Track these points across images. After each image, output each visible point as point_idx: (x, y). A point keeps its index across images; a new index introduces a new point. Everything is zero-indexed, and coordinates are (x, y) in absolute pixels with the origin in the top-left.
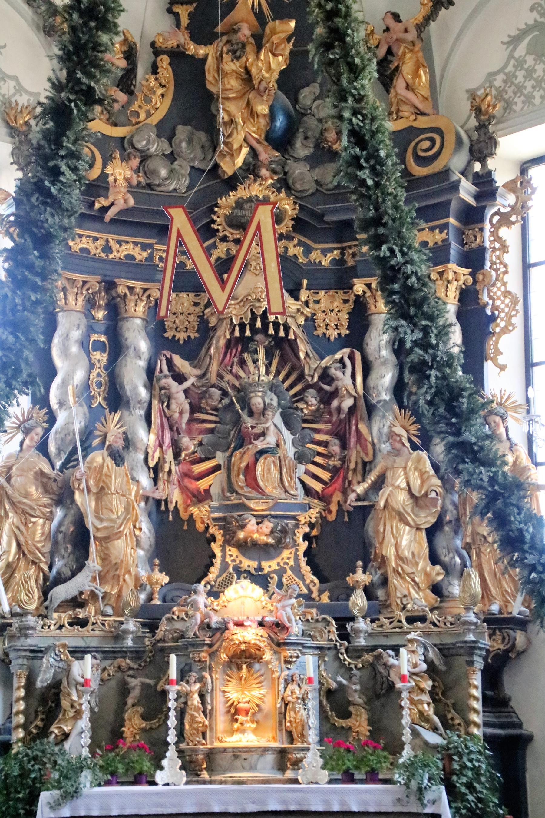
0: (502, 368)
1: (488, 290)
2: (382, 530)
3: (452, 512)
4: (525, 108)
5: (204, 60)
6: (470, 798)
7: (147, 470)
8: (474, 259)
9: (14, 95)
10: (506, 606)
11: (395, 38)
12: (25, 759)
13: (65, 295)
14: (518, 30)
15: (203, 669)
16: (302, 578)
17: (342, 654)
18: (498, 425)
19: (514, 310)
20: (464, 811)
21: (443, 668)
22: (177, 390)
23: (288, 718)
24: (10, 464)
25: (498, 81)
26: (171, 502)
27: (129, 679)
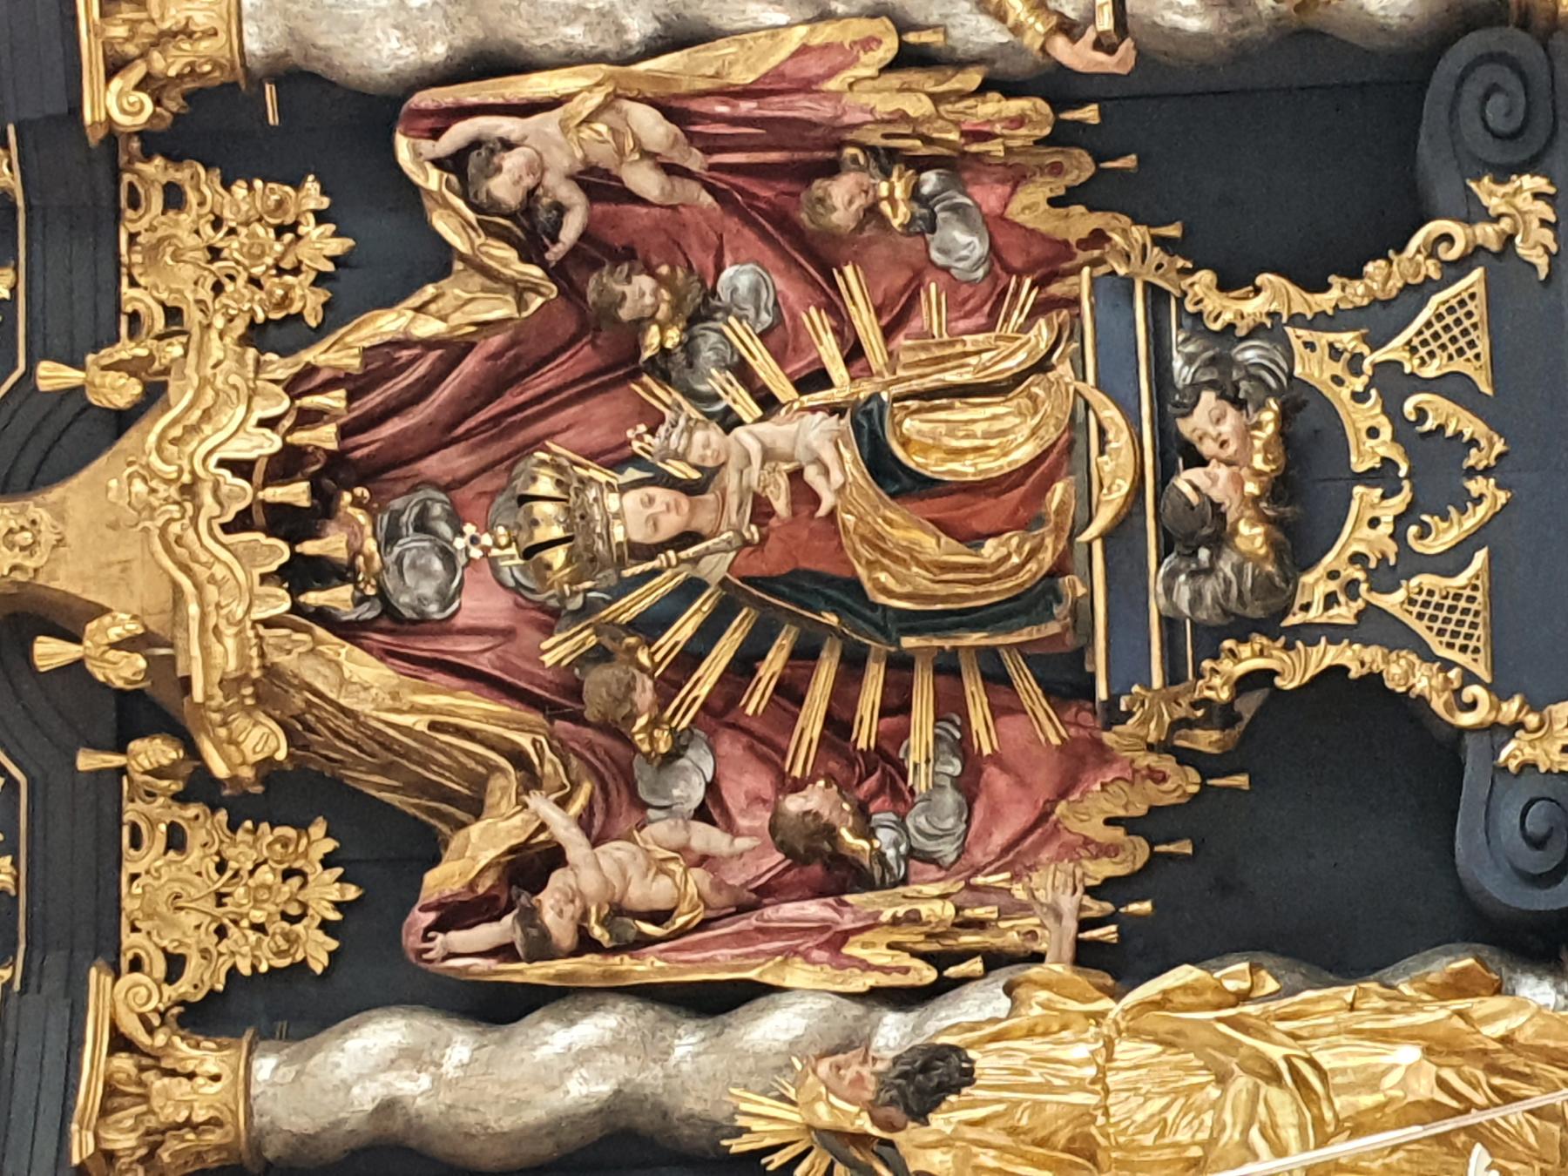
16: (1417, 292)
22: (591, 872)
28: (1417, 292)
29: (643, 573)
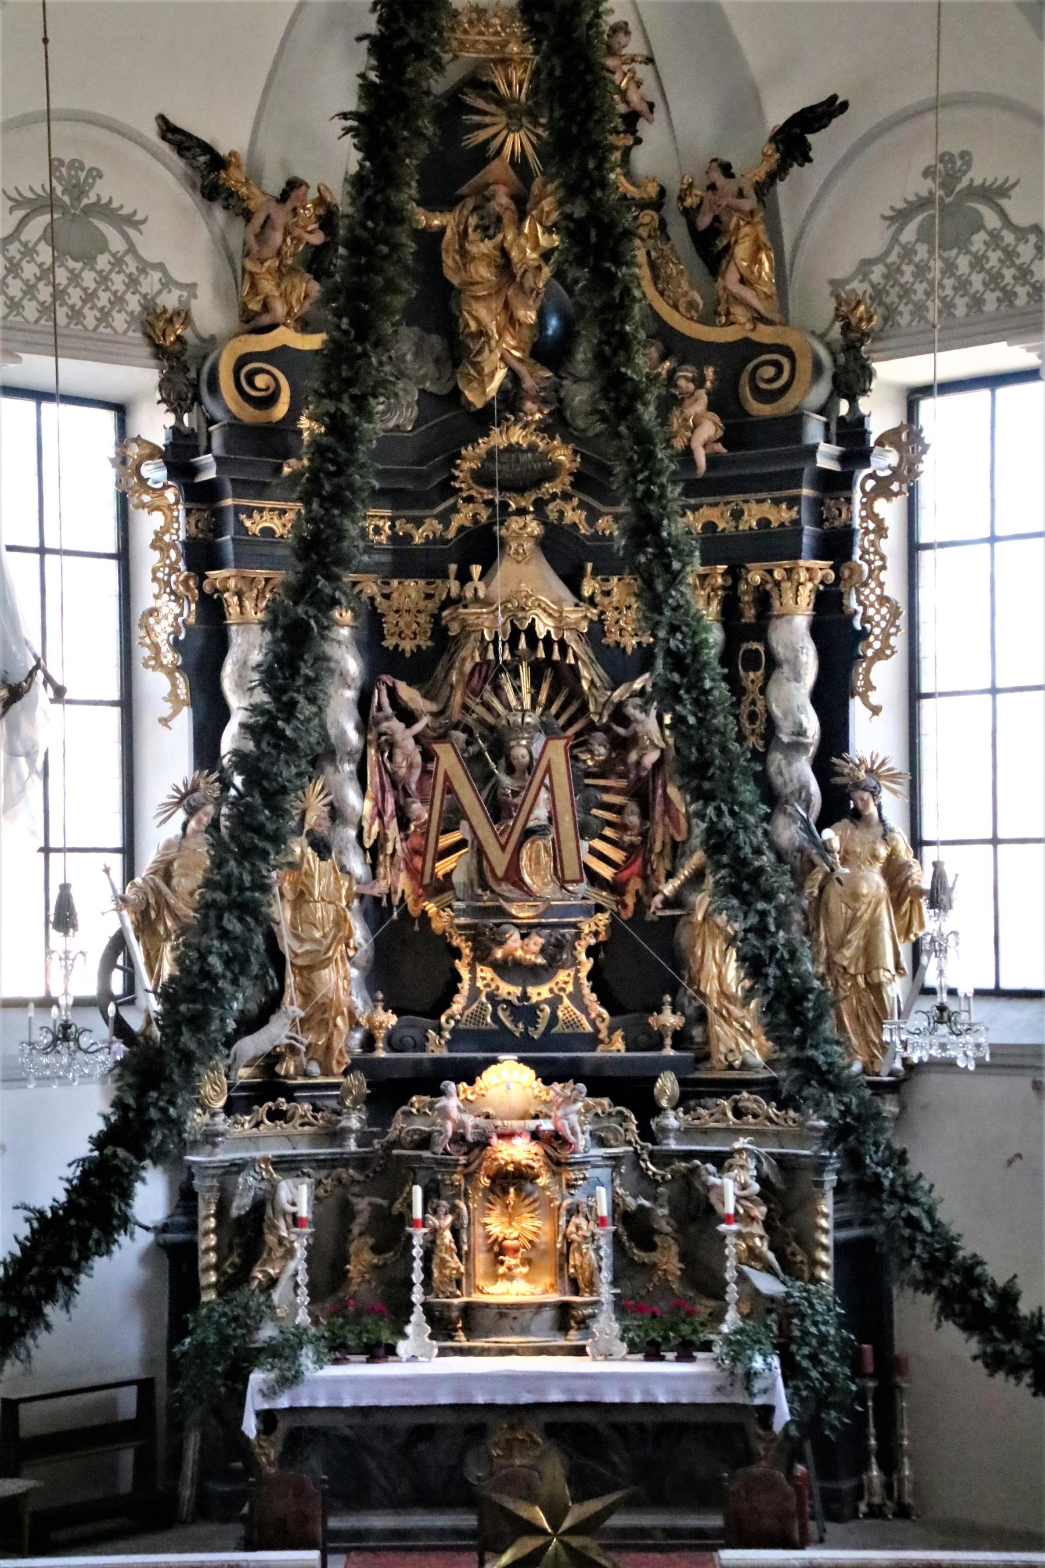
0: (876, 710)
1: (858, 593)
2: (699, 953)
3: (799, 924)
4: (915, 323)
6: (814, 1374)
7: (361, 851)
8: (836, 545)
9: (160, 292)
10: (872, 1063)
11: (724, 203)
12: (223, 1320)
13: (240, 600)
14: (906, 201)
15: (457, 1196)
16: (585, 1010)
17: (644, 1160)
18: (866, 804)
19: (893, 625)
20: (804, 1393)
21: (780, 1186)
22: (404, 736)
23: (572, 1262)
24: (169, 857)
25: (877, 273)
26: (396, 892)
27: (354, 1200)
28: (585, 1010)
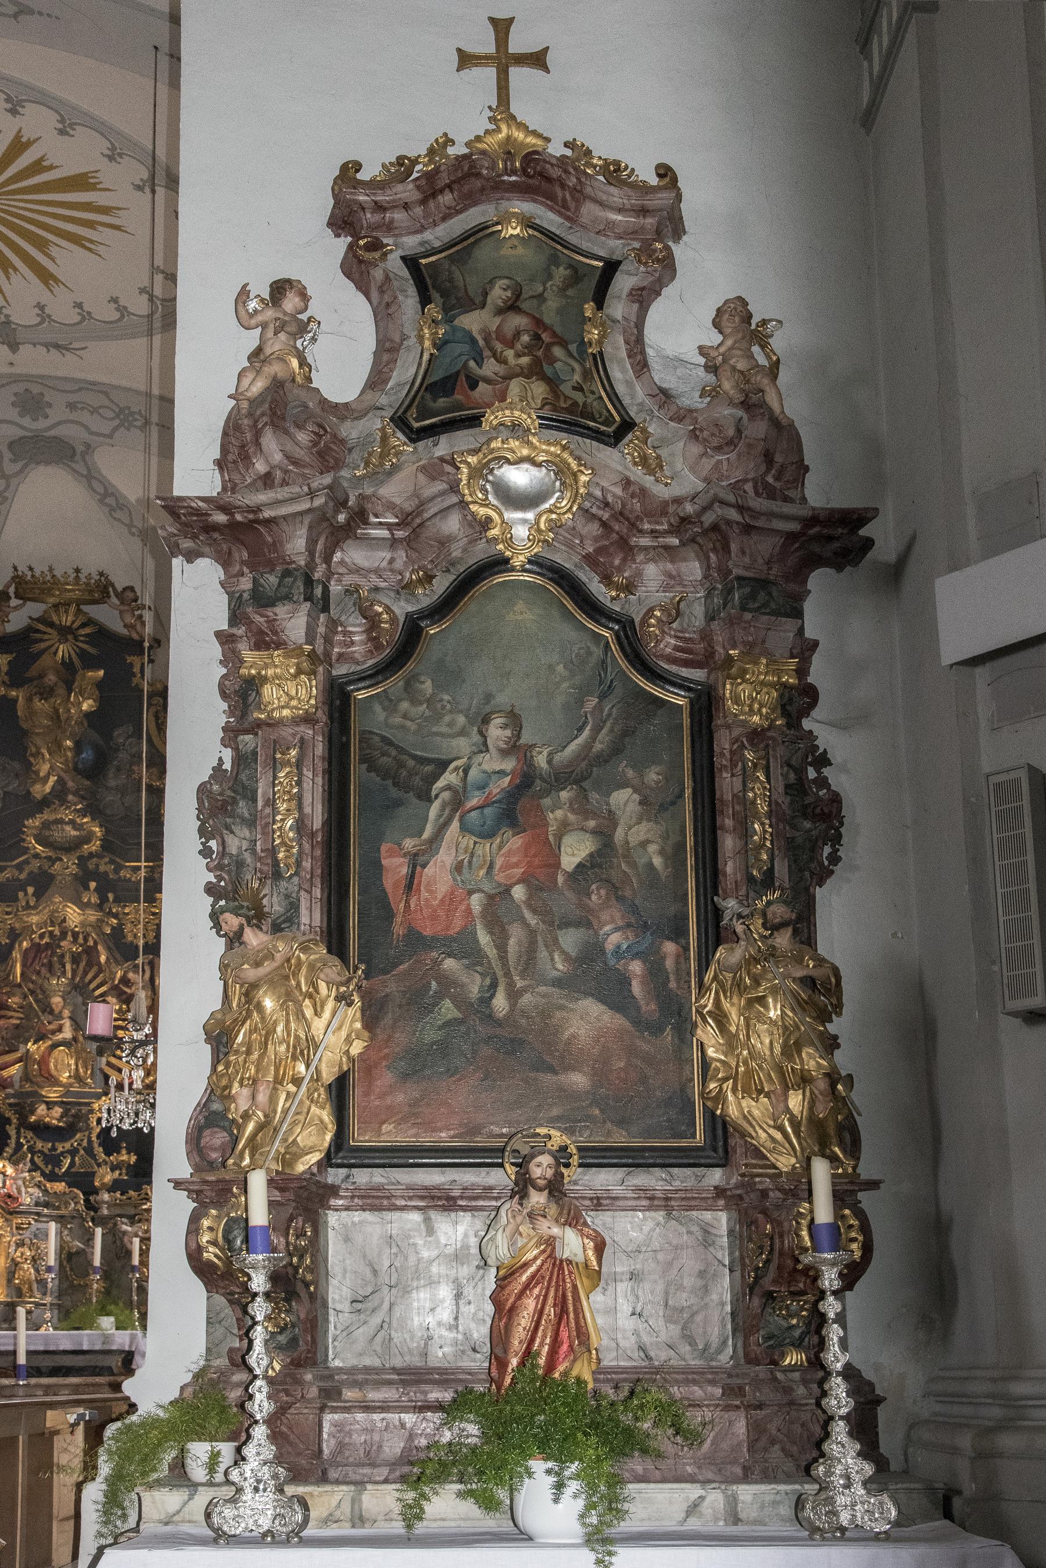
5: (15, 701)
29: (21, 180)
